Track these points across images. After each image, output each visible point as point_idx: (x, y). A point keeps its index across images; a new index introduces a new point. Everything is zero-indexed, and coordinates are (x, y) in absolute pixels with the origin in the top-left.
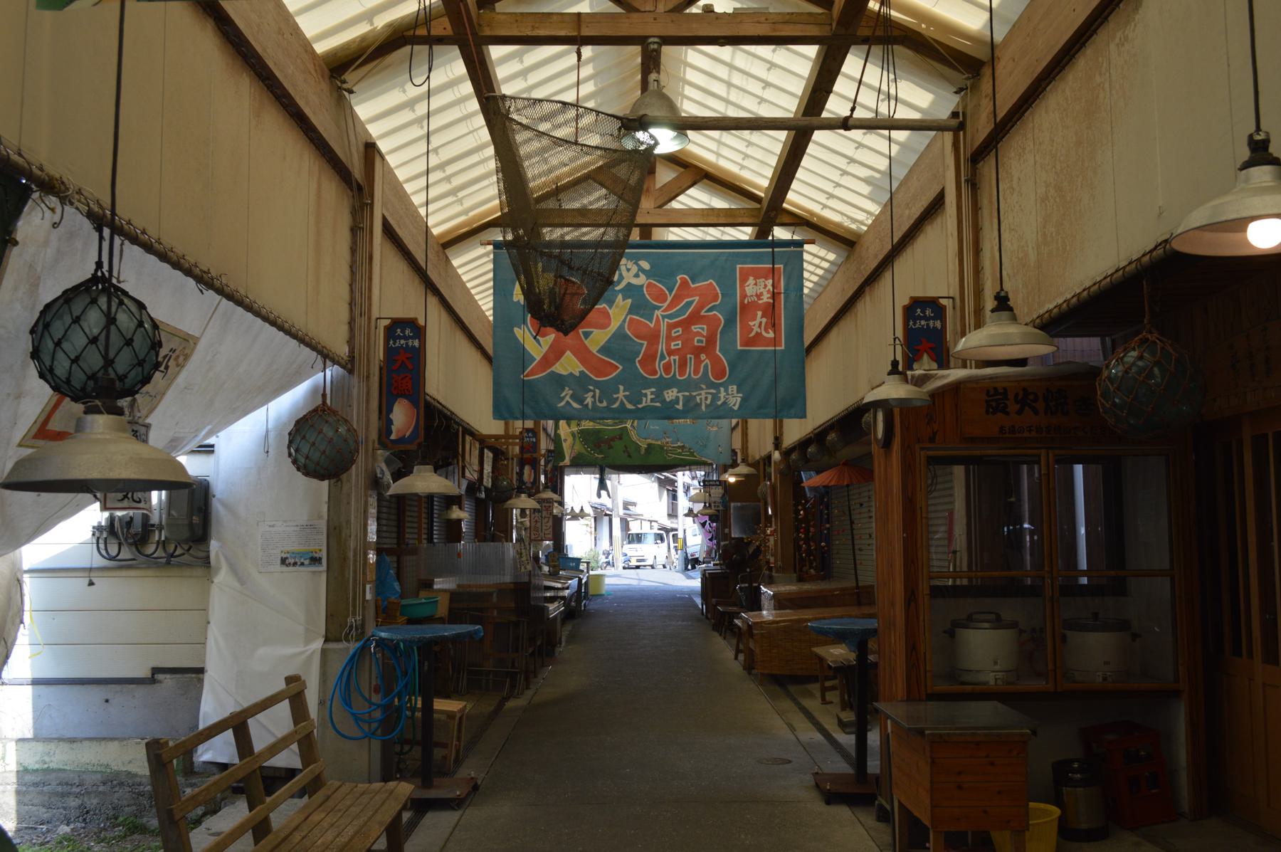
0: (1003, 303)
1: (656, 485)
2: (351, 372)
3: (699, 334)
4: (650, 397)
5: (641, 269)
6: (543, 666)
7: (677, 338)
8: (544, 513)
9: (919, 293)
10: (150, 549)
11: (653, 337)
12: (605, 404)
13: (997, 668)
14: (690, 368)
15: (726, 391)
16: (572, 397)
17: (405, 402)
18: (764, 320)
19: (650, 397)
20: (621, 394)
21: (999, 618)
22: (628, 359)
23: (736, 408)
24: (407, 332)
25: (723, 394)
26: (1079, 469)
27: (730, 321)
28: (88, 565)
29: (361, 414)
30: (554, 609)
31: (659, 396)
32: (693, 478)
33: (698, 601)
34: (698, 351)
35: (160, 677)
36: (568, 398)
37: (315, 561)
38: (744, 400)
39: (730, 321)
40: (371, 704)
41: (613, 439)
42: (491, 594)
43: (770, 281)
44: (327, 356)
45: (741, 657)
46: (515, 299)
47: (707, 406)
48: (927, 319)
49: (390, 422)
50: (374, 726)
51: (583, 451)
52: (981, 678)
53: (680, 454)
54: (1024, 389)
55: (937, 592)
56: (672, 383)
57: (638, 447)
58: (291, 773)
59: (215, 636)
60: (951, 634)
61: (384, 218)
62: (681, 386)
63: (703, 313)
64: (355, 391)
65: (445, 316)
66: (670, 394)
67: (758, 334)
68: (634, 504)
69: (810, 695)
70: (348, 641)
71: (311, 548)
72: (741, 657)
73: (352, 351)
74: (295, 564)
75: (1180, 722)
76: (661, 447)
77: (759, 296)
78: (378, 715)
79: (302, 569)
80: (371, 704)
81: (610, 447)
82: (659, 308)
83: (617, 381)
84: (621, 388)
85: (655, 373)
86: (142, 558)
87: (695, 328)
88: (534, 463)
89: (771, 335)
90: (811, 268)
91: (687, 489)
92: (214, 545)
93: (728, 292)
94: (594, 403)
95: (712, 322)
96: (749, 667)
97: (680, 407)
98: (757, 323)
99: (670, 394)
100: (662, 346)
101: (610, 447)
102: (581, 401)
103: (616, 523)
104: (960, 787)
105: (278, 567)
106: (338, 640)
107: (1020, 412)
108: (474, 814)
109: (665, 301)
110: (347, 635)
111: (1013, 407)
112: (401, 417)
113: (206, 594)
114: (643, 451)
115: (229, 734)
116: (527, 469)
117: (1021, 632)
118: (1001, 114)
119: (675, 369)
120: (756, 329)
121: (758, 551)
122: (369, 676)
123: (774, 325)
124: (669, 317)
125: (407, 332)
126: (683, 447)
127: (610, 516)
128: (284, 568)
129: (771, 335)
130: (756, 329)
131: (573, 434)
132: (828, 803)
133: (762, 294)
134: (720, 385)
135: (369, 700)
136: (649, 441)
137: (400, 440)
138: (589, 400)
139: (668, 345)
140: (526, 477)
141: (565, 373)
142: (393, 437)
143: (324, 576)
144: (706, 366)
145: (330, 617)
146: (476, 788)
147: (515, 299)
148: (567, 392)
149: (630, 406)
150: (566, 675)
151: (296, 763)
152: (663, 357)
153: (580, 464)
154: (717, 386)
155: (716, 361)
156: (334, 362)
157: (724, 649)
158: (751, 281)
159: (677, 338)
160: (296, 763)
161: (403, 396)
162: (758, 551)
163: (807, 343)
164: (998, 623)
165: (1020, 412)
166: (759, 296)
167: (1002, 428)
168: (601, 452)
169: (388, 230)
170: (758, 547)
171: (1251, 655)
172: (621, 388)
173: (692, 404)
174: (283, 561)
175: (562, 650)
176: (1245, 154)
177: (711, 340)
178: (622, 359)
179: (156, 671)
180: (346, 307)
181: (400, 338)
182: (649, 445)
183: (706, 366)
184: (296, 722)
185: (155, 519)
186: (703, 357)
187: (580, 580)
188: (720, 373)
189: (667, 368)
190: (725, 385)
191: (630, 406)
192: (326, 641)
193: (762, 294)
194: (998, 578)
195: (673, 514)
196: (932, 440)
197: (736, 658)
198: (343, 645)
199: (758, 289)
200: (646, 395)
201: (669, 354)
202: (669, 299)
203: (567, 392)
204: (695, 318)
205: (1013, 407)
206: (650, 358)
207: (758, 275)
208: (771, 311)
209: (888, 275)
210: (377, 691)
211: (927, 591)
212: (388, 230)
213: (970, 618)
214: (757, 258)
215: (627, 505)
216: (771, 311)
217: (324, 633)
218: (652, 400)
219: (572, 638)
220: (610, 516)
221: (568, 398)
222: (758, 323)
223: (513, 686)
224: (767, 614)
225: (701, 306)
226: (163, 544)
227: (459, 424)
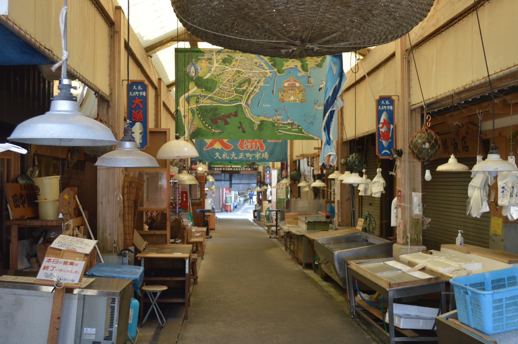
9: (382, 94)
25: (263, 155)
41: (229, 116)
48: (386, 105)
51: (202, 127)
53: (289, 130)
56: (248, 151)
57: (252, 123)
61: (163, 102)
62: (251, 153)
76: (273, 124)
81: (226, 123)
101: (226, 123)
114: (256, 127)
118: (357, 79)
126: (292, 124)
131: (193, 111)
136: (262, 118)
168: (218, 128)
203: (217, 154)
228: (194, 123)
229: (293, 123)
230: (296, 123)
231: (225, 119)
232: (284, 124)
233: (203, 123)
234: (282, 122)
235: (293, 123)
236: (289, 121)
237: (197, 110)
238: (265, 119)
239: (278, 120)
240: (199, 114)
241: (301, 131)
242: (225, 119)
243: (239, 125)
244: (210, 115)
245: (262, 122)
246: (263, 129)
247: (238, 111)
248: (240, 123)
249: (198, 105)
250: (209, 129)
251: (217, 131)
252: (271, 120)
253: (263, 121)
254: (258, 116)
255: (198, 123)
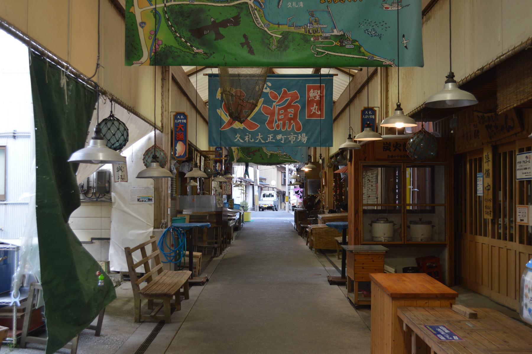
0: (399, 107)
1: (276, 169)
2: (162, 132)
3: (290, 112)
4: (271, 138)
5: (268, 86)
6: (226, 247)
7: (282, 114)
8: (228, 183)
10: (90, 195)
11: (272, 114)
12: (253, 140)
13: (385, 236)
14: (287, 126)
15: (301, 135)
16: (240, 137)
17: (181, 142)
18: (317, 107)
19: (271, 138)
20: (260, 137)
21: (387, 220)
22: (262, 122)
23: (305, 142)
24: (182, 117)
25: (300, 137)
26: (409, 171)
27: (303, 108)
28: (7, 206)
29: (166, 146)
30: (232, 224)
31: (274, 137)
32: (295, 167)
33: (293, 224)
34: (290, 119)
35: (94, 241)
36: (238, 138)
37: (150, 200)
38: (308, 139)
39: (303, 108)
40: (171, 250)
41: (255, 151)
42: (206, 216)
43: (319, 92)
44: (155, 127)
45: (308, 245)
46: (217, 98)
47: (293, 142)
49: (176, 150)
50: (172, 258)
51: (242, 157)
52: (380, 239)
54: (396, 143)
55: (365, 212)
57: (266, 155)
58: (142, 274)
59: (114, 225)
60: (371, 225)
63: (292, 104)
64: (164, 139)
65: (175, 88)
66: (279, 137)
67: (314, 113)
68: (265, 179)
69: (334, 256)
70: (162, 228)
71: (148, 195)
72: (308, 245)
73: (162, 124)
74: (143, 201)
75: (446, 254)
76: (277, 155)
77: (315, 97)
78: (173, 254)
79: (145, 203)
80: (171, 250)
81: (220, 36)
82: (274, 102)
83: (257, 132)
84: (260, 134)
85: (273, 128)
86: (88, 199)
87: (289, 110)
88: (221, 162)
89: (319, 113)
90: (336, 82)
91: (291, 171)
92: (113, 194)
93: (303, 95)
94: (249, 140)
95: (296, 108)
96: (311, 248)
97: (283, 142)
98: (314, 108)
99: (279, 137)
100: (276, 117)
101: (220, 36)
102: (243, 139)
103: (256, 188)
104: (363, 268)
105: (136, 202)
106: (158, 228)
107: (395, 150)
108: (207, 286)
109: (277, 99)
110: (162, 226)
111: (392, 149)
112: (180, 148)
113: (110, 212)
114: (268, 157)
115: (139, 250)
116: (218, 164)
117: (394, 224)
119: (281, 126)
120: (314, 111)
121: (319, 201)
122: (169, 241)
123: (320, 109)
124: (279, 105)
125: (182, 117)
126: (286, 155)
127: (253, 185)
128: (139, 203)
129: (319, 113)
130: (314, 111)
132: (331, 284)
133: (316, 96)
134: (299, 133)
135: (170, 249)
136: (271, 152)
137: (180, 157)
138: (247, 139)
139: (278, 117)
140: (217, 168)
141: (237, 128)
142: (177, 155)
143: (153, 205)
144: (293, 125)
145: (155, 220)
146: (207, 280)
147: (217, 98)
148: (238, 135)
149: (263, 142)
150: (235, 248)
151: (144, 272)
152: (276, 122)
153: (239, 161)
154: (297, 134)
155: (297, 123)
156: (157, 129)
157: (302, 243)
158: (312, 91)
159: (282, 114)
160: (144, 272)
161: (181, 141)
162: (319, 201)
163: (333, 118)
164: (387, 221)
165: (395, 150)
166: (315, 97)
167: (388, 156)
168: (250, 157)
169: (174, 79)
170: (319, 200)
171: (515, 242)
172: (260, 134)
173: (287, 141)
174: (138, 200)
175: (233, 242)
176: (396, 107)
177: (295, 115)
178: (260, 123)
179: (93, 239)
180: (160, 108)
181: (179, 119)
182: (271, 154)
183: (293, 125)
184: (143, 257)
185: (91, 184)
186: (292, 122)
187: (240, 213)
188: (299, 129)
189: (278, 126)
190: (301, 133)
191: (263, 142)
192: (154, 228)
193: (316, 96)
194: (390, 208)
195: (284, 184)
196: (365, 160)
197: (307, 245)
198: (161, 230)
199: (314, 94)
200: (269, 137)
201: (279, 121)
202: (279, 98)
204: (289, 106)
205: (392, 149)
206: (271, 122)
207: (315, 88)
208: (319, 103)
209: (366, 88)
210: (173, 245)
211: (362, 210)
212: (174, 79)
213: (378, 220)
214: (314, 82)
215: (261, 180)
216: (319, 103)
217: (153, 225)
218: (272, 139)
219: (237, 238)
220: (253, 185)
221: (238, 138)
222: (314, 108)
223: (215, 254)
224: (320, 225)
225: (292, 101)
226: (94, 194)
227: (193, 147)
228: (239, 155)
229: (344, 35)
230: (288, 154)
231: (253, 153)
232: (326, 38)
233: (176, 37)
234: (324, 35)
235: (344, 35)
236: (336, 32)
237: (166, 13)
238: (292, 29)
239: (316, 31)
240: (168, 20)
241: (290, 158)
242: (253, 153)
243: (243, 41)
244: (188, 22)
245: (285, 35)
246: (287, 47)
247: (242, 15)
248: (245, 36)
249: (167, 4)
250: (188, 48)
251: (201, 51)
252: (302, 31)
253: (288, 33)
254: (279, 24)
255: (166, 37)
